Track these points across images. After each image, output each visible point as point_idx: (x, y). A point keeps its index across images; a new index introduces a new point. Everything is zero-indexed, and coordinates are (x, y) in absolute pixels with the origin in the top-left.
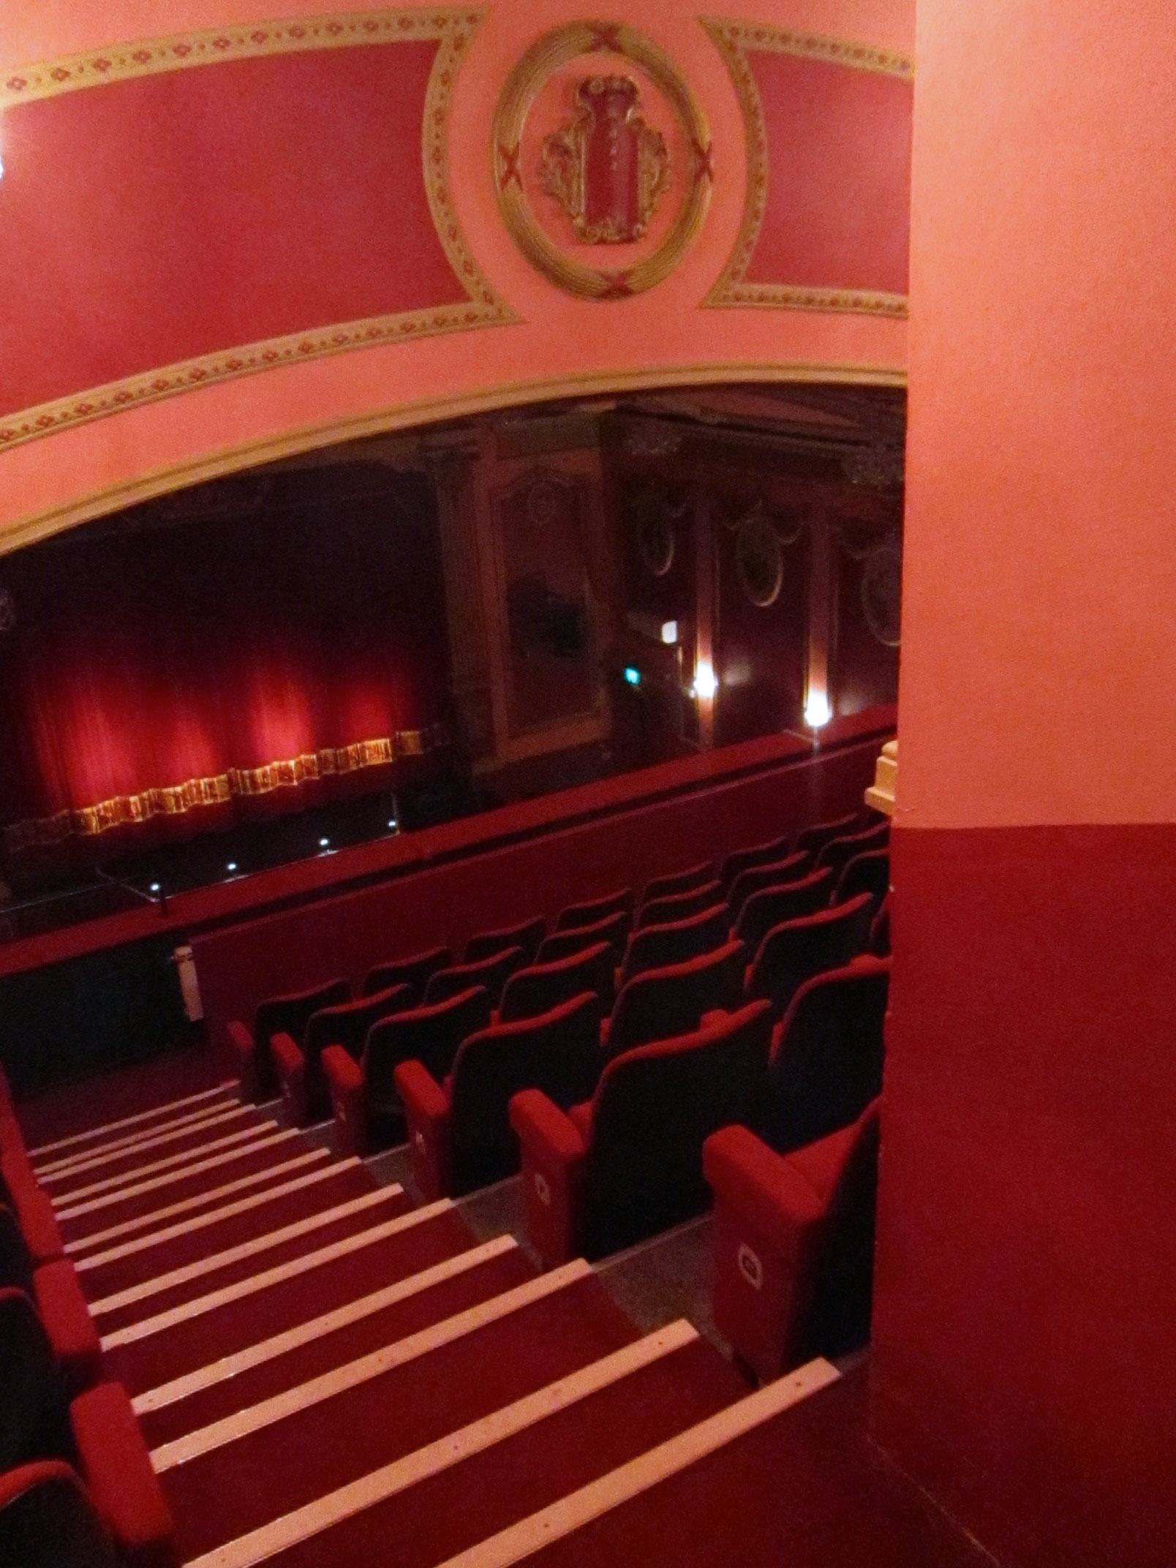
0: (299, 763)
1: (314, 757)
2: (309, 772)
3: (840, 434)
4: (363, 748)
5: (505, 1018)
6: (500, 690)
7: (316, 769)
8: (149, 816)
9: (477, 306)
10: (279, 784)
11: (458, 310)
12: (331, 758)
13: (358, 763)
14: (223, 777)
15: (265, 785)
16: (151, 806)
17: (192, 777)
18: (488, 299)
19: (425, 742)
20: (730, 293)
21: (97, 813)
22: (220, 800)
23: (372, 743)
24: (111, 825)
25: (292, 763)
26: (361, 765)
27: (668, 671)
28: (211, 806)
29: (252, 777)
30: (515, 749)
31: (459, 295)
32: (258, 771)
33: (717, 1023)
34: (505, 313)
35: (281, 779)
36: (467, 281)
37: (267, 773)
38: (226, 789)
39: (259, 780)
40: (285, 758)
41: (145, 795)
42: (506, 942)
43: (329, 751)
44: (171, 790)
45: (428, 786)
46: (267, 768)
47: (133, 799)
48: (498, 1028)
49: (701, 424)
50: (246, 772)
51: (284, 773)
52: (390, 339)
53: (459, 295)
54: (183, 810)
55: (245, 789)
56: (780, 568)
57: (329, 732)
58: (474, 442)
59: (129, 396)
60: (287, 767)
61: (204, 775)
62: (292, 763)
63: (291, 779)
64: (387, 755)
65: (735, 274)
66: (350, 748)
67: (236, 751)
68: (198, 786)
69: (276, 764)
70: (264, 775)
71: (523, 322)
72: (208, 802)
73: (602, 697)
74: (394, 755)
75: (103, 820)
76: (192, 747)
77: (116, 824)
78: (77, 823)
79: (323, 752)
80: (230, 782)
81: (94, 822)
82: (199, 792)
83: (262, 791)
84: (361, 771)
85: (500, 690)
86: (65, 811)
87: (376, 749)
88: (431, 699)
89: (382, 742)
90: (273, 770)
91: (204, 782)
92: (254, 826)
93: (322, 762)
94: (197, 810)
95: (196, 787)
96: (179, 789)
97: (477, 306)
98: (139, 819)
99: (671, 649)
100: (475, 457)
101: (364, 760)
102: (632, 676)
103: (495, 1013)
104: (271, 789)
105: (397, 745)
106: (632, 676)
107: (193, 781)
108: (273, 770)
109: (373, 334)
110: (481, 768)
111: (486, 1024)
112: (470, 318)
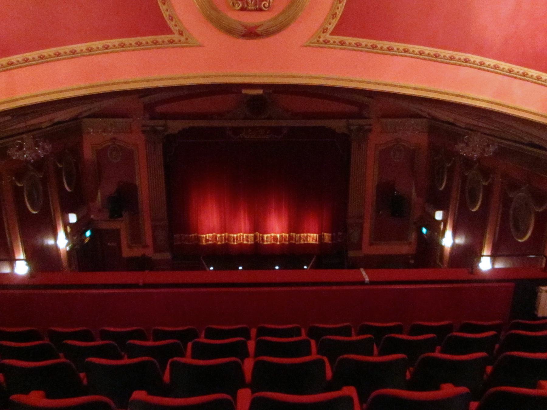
0: (281, 236)
1: (287, 235)
2: (285, 240)
3: (488, 132)
4: (307, 236)
5: (442, 352)
6: (368, 225)
7: (287, 239)
8: (223, 243)
9: (176, 37)
10: (273, 242)
11: (166, 38)
12: (294, 237)
13: (304, 241)
14: (252, 235)
15: (267, 241)
16: (225, 239)
17: (215, 232)
18: (181, 33)
19: (332, 238)
20: (321, 40)
21: (207, 237)
22: (249, 243)
23: (312, 235)
24: (210, 242)
25: (278, 236)
26: (306, 242)
27: (437, 230)
28: (245, 244)
29: (263, 237)
30: (368, 249)
31: (167, 30)
32: (265, 236)
33: (448, 390)
34: (189, 40)
35: (274, 240)
36: (171, 24)
37: (268, 238)
38: (253, 239)
39: (265, 239)
40: (276, 233)
41: (223, 235)
42: (105, 335)
43: (294, 234)
44: (232, 235)
45: (321, 256)
46: (269, 235)
47: (218, 235)
48: (437, 354)
49: (455, 125)
50: (261, 235)
51: (275, 238)
52: (130, 48)
53: (167, 30)
54: (235, 243)
55: (240, 240)
56: (481, 195)
57: (295, 226)
58: (370, 125)
59: (12, 64)
60: (276, 236)
61: (245, 233)
62: (278, 236)
63: (277, 241)
64: (316, 241)
65: (325, 31)
66: (302, 235)
67: (258, 226)
68: (243, 236)
69: (273, 235)
70: (267, 237)
71: (203, 46)
72: (245, 242)
73: (413, 237)
74: (319, 241)
75: (207, 240)
76: (244, 222)
77: (212, 242)
78: (198, 239)
79: (291, 234)
80: (255, 237)
81: (204, 241)
82: (243, 238)
83: (265, 243)
84: (305, 244)
85: (368, 225)
86: (196, 234)
87: (312, 238)
88: (338, 223)
89: (315, 235)
90: (271, 236)
91: (245, 235)
92: (258, 256)
93: (291, 238)
94: (241, 245)
95: (242, 236)
96: (235, 235)
97: (176, 37)
98: (219, 243)
99: (439, 222)
100: (370, 130)
101: (307, 241)
102: (424, 230)
103: (439, 348)
104: (269, 243)
105: (321, 238)
106: (424, 230)
107: (242, 234)
108: (271, 236)
109: (122, 45)
110: (352, 254)
111: (434, 351)
112: (171, 42)
